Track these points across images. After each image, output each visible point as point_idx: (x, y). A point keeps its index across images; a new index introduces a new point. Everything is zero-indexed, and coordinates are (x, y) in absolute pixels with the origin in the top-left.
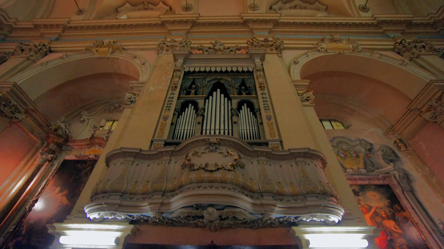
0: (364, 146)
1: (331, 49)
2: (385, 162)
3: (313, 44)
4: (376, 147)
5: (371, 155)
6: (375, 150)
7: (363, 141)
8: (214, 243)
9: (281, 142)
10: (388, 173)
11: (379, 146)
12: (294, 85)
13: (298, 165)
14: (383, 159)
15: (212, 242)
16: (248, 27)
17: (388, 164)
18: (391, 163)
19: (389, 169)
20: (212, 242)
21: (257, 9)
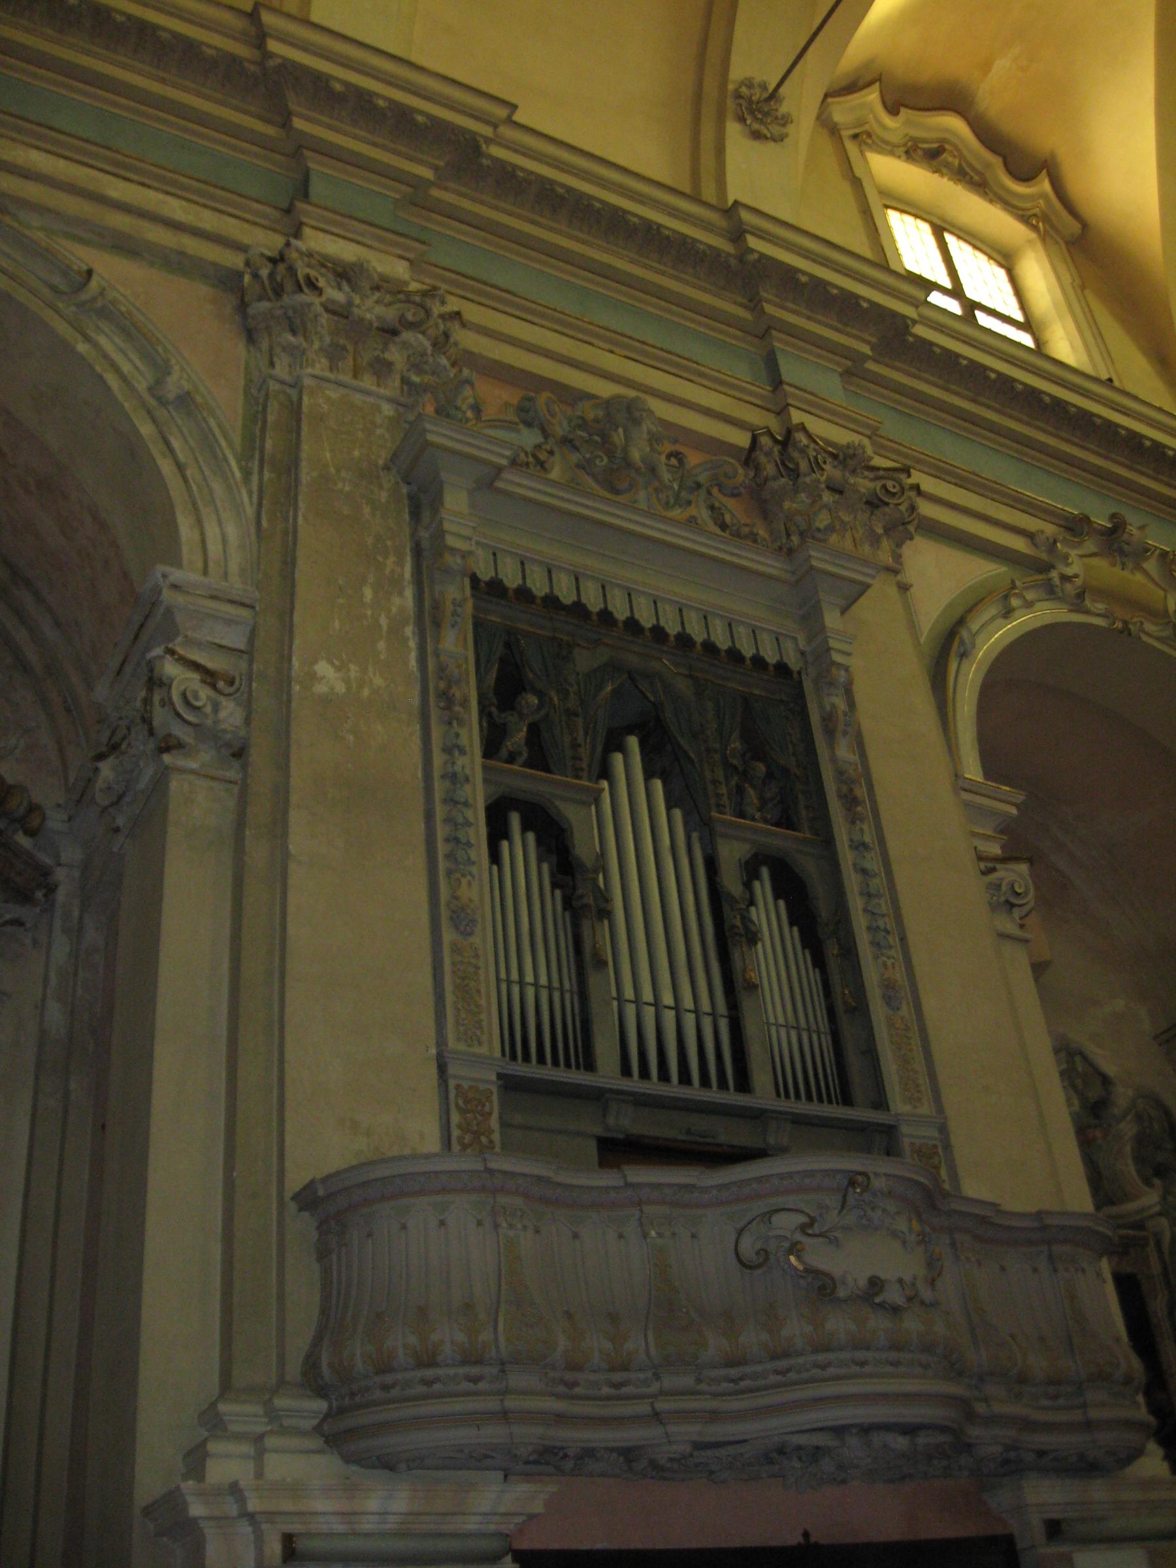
0: (1079, 1082)
1: (1103, 593)
2: (1138, 1171)
3: (1030, 536)
4: (1122, 1096)
5: (1098, 1133)
6: (1116, 1111)
7: (1078, 1059)
8: (813, 1540)
9: (943, 1129)
10: (1140, 1226)
11: (1130, 1092)
12: (967, 805)
13: (1056, 1270)
14: (1139, 1160)
15: (806, 1535)
16: (754, 304)
17: (1147, 1182)
18: (1157, 1182)
19: (1143, 1210)
20: (806, 1535)
21: (776, 129)
